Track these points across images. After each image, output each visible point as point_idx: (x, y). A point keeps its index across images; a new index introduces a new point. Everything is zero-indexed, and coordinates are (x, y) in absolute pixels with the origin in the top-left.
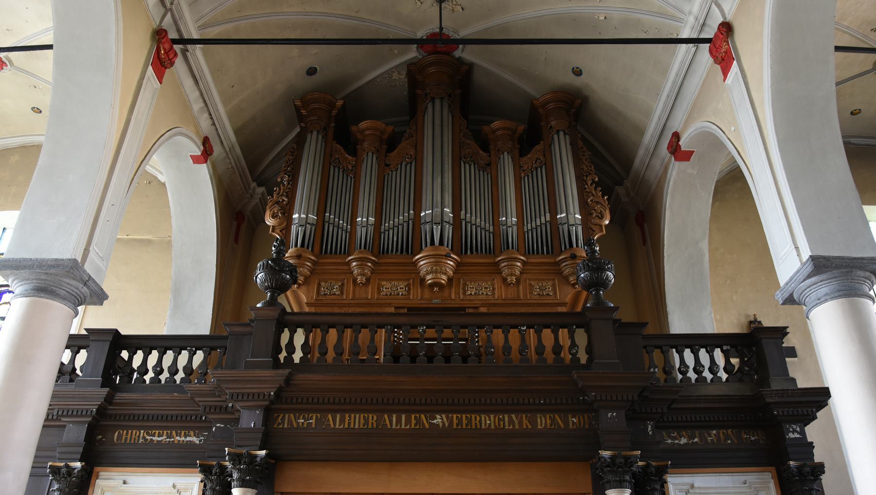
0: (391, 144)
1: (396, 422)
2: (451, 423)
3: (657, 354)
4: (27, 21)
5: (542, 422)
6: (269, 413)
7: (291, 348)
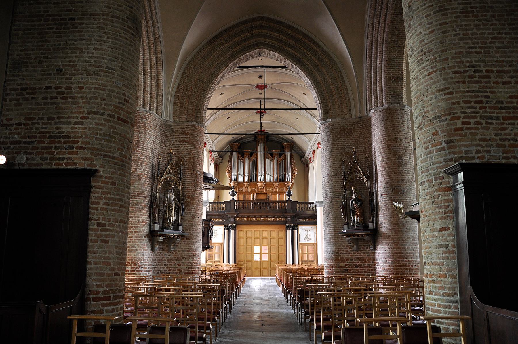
0: (251, 154)
1: (255, 219)
5: (278, 219)
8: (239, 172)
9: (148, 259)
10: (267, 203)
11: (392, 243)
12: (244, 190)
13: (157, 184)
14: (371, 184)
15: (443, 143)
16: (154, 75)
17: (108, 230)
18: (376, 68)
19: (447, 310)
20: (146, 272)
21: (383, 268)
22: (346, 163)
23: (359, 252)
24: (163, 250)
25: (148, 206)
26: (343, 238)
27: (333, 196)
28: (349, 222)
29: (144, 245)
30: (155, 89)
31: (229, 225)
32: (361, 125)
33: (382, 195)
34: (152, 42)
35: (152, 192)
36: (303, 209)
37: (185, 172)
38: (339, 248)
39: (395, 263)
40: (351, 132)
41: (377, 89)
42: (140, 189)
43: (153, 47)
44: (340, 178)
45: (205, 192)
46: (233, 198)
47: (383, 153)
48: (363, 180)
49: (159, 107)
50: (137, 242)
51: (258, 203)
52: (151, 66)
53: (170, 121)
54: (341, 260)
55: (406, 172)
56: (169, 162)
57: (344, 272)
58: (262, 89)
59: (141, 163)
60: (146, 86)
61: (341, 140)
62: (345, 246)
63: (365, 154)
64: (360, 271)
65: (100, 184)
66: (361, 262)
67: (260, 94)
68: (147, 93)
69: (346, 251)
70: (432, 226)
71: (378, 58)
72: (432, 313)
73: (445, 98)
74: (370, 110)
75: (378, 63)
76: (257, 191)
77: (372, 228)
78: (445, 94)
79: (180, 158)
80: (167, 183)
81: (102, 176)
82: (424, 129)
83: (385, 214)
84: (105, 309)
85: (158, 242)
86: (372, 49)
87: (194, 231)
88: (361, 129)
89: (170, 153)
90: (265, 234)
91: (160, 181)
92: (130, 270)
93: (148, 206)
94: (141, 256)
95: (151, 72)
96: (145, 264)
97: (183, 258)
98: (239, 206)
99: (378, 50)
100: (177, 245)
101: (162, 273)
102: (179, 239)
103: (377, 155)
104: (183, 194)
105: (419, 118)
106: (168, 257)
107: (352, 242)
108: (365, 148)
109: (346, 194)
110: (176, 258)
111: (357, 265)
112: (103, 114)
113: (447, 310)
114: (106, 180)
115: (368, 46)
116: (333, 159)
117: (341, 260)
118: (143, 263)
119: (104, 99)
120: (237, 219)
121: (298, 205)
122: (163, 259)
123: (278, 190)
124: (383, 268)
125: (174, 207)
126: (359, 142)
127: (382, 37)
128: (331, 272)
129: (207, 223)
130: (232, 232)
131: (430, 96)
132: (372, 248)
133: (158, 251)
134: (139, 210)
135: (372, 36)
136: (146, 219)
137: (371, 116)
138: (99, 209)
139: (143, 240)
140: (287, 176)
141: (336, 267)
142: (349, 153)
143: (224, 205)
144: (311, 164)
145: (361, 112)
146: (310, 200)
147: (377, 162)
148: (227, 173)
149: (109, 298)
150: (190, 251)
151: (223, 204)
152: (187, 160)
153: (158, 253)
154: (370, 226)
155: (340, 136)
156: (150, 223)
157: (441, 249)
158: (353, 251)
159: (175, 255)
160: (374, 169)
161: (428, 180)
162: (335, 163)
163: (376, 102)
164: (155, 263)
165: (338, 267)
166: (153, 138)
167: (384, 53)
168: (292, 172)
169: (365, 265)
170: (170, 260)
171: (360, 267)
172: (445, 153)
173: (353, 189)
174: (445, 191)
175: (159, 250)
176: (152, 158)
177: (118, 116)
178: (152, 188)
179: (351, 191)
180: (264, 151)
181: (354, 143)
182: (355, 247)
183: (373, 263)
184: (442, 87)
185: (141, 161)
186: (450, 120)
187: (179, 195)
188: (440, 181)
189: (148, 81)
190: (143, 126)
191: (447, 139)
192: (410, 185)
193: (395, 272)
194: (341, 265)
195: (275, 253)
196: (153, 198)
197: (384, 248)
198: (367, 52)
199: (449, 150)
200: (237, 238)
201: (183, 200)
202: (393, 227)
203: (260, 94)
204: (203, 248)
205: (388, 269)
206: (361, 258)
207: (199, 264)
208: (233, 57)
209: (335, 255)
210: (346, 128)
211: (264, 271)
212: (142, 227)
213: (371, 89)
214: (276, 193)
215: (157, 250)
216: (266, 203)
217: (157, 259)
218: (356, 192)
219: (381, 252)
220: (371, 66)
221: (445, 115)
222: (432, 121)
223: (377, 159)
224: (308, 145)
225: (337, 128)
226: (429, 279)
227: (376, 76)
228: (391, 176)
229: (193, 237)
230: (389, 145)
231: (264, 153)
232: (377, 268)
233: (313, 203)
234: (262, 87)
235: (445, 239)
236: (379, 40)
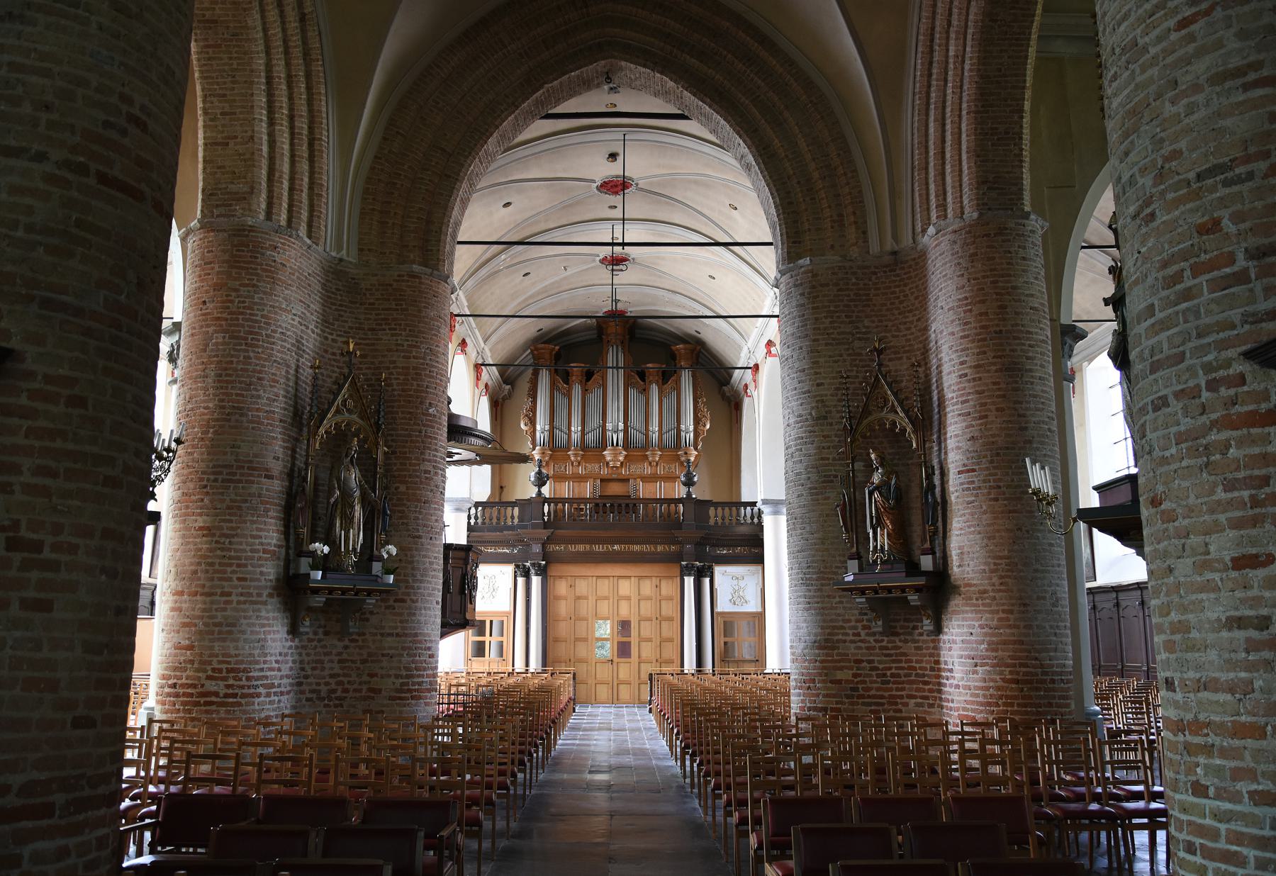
0: (589, 375)
1: (598, 548)
2: (133, 730)
3: (712, 508)
4: (710, 276)
5: (660, 548)
6: (543, 545)
7: (513, 517)
8: (557, 423)
9: (279, 658)
10: (631, 506)
11: (992, 612)
12: (569, 470)
13: (308, 441)
14: (923, 441)
15: (1240, 256)
16: (302, 125)
17: (53, 566)
18: (944, 108)
19: (1268, 855)
20: (273, 698)
21: (966, 687)
22: (854, 383)
23: (893, 638)
24: (326, 633)
25: (279, 505)
26: (845, 597)
27: (814, 477)
28: (862, 552)
29: (268, 619)
30: (304, 166)
31: (528, 564)
32: (898, 275)
33: (960, 473)
34: (293, 24)
35: (293, 464)
36: (727, 521)
37: (393, 407)
38: (834, 627)
39: (1001, 673)
40: (868, 295)
41: (944, 169)
42: (256, 456)
43: (295, 40)
44: (836, 427)
45: (451, 472)
46: (539, 491)
47: (962, 350)
48: (903, 430)
49: (315, 219)
50: (244, 611)
51: (605, 505)
52: (291, 98)
53: (351, 263)
54: (839, 661)
55: (1032, 406)
56: (346, 379)
57: (848, 697)
58: (616, 193)
59: (260, 379)
60: (278, 156)
61: (838, 317)
62: (849, 621)
63: (909, 358)
64: (894, 693)
65: (24, 400)
66: (897, 668)
67: (611, 207)
68: (281, 177)
69: (854, 635)
70: (1202, 550)
71: (950, 78)
72: (1204, 862)
73: (1244, 102)
74: (924, 231)
75: (949, 91)
76: (605, 472)
77: (931, 569)
78: (1246, 87)
79: (378, 368)
80: (339, 438)
81: (30, 375)
82: (1162, 218)
83: (969, 527)
84: (27, 851)
85: (310, 610)
86: (932, 51)
87: (419, 577)
88: (896, 286)
89: (348, 352)
90: (626, 587)
91: (316, 433)
92: (222, 692)
93: (279, 505)
94: (257, 652)
95: (291, 118)
96: (269, 673)
97: (383, 655)
98: (555, 511)
99: (951, 53)
100: (368, 616)
101: (324, 699)
102: (371, 601)
103: (946, 359)
104: (387, 471)
105: (1141, 181)
106: (339, 654)
107: (872, 610)
108: (910, 340)
109: (853, 471)
110: (365, 657)
111: (885, 675)
112: (41, 157)
113: (1268, 855)
114: (49, 387)
115: (920, 44)
116: (816, 373)
117: (839, 661)
118: (262, 670)
119: (47, 108)
120: (552, 548)
121: (712, 511)
122: (327, 658)
123: (661, 471)
124: (966, 687)
125: (358, 508)
126: (890, 324)
127: (964, 12)
128: (808, 695)
129: (462, 554)
130: (536, 581)
131: (1185, 101)
132: (931, 628)
133: (311, 636)
134: (253, 515)
135: (934, 13)
136: (274, 541)
137: (925, 246)
138: (17, 488)
139: (265, 603)
140: (683, 434)
141: (823, 681)
142: (860, 354)
143: (516, 510)
144: (746, 401)
145: (896, 237)
146: (745, 498)
147: (945, 378)
148: (523, 426)
149: (48, 811)
150: (406, 635)
151: (513, 507)
152: (398, 374)
153: (310, 640)
154: (927, 562)
155: (836, 307)
156: (287, 554)
157: (1241, 635)
158: (874, 634)
159: (361, 648)
160: (935, 398)
161: (1183, 390)
162: (822, 384)
163: (942, 206)
164: (303, 669)
165: (831, 682)
166: (298, 309)
167: (968, 62)
168: (697, 421)
169: (910, 675)
170: (347, 661)
171: (894, 683)
172: (1251, 290)
173: (873, 456)
174: (1253, 426)
175: (315, 633)
176: (293, 366)
177: (101, 168)
178: (294, 451)
179: (869, 463)
180: (621, 364)
181: (877, 327)
182: (880, 623)
183: (932, 669)
184: (1235, 62)
185: (260, 372)
186: (1266, 176)
187: (376, 473)
188: (1232, 392)
189: (283, 143)
190: (266, 271)
191: (1253, 241)
192: (1042, 443)
193: (1001, 697)
194: (840, 675)
195: (650, 640)
196: (296, 481)
197: (969, 626)
198: (916, 62)
199: (1264, 280)
200: (551, 597)
201: (386, 488)
202: (992, 567)
203: (611, 207)
204: (444, 625)
205: (982, 688)
206: (897, 655)
207: (431, 672)
208: (530, 84)
209: (820, 648)
210: (853, 284)
211: (621, 687)
212: (262, 566)
213: (927, 169)
214: (653, 478)
215: (307, 633)
216: (627, 505)
217: (306, 659)
218: (882, 465)
219: (959, 639)
220: (928, 104)
221: (1248, 159)
222: (1194, 186)
223: (946, 368)
224: (740, 348)
225: (827, 285)
226: (1189, 738)
227: (944, 131)
228: (986, 417)
229: (415, 594)
230: (982, 327)
231: (622, 371)
232: (945, 685)
233: (753, 504)
234: (616, 186)
235: (1253, 599)
236: (955, 22)
